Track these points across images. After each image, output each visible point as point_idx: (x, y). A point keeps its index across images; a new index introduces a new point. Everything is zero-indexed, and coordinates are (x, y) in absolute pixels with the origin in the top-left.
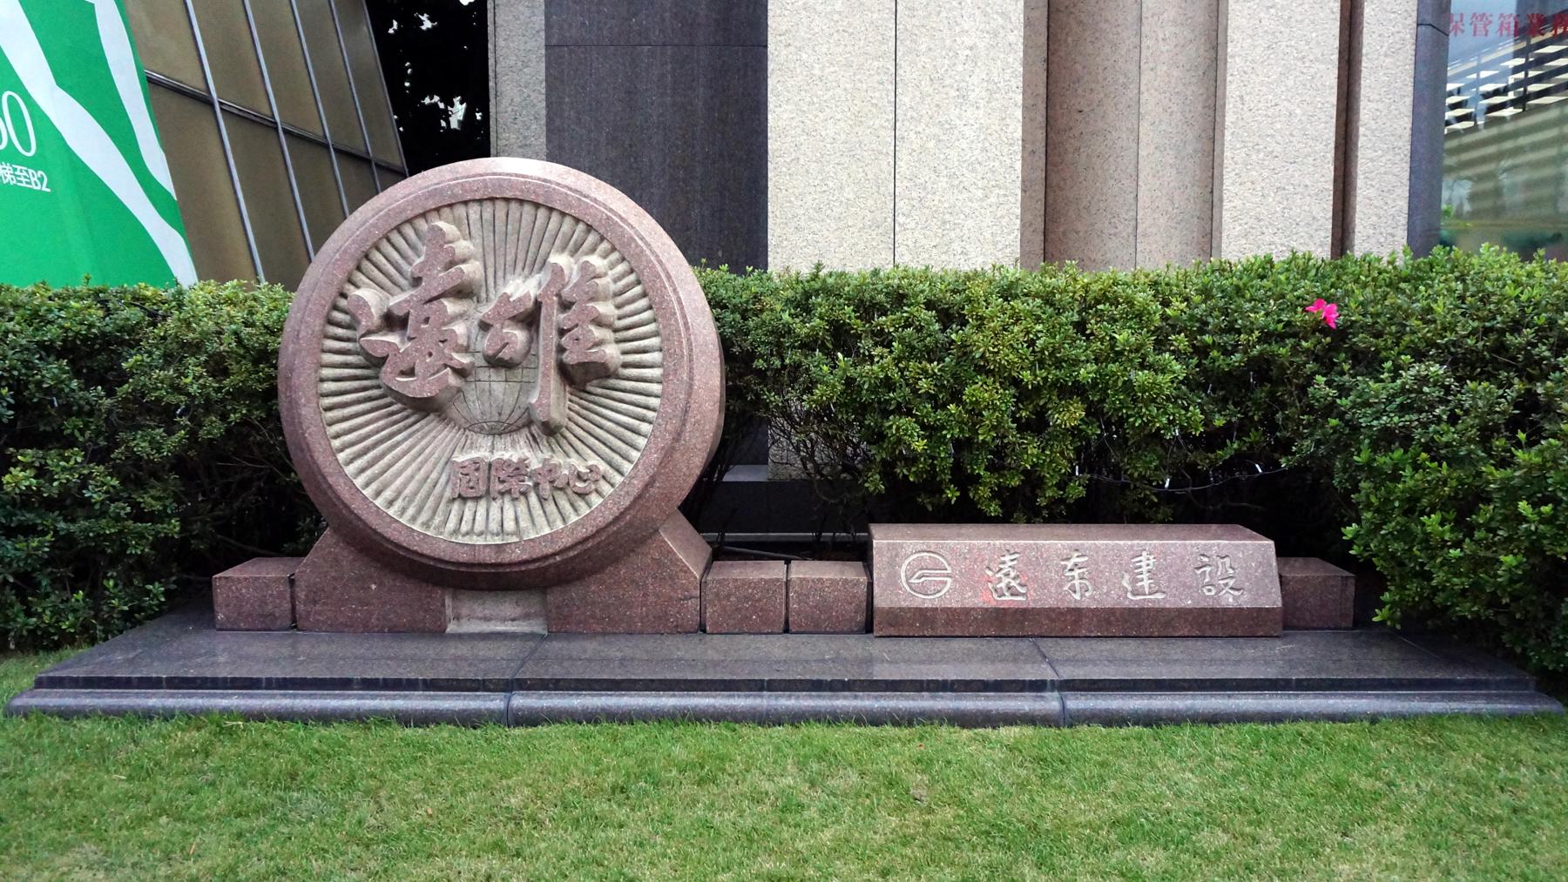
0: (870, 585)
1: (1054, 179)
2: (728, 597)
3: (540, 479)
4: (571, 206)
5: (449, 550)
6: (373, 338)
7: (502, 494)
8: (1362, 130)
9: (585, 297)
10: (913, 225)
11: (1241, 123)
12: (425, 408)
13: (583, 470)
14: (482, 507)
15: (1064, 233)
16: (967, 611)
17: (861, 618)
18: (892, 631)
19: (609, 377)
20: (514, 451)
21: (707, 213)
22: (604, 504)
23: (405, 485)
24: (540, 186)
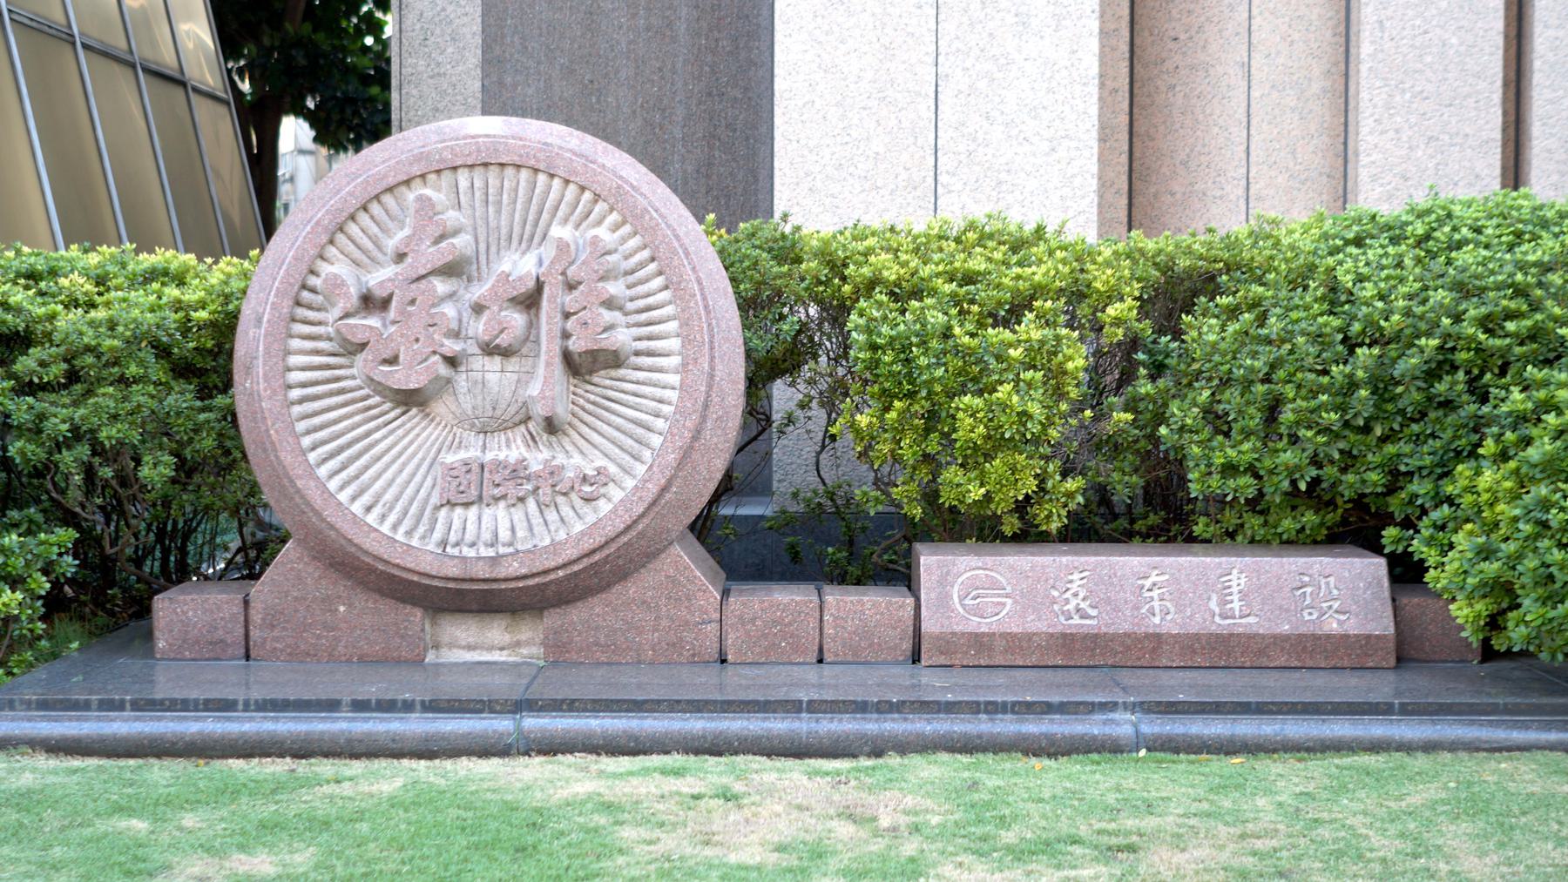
0: (918, 607)
1: (1140, 128)
2: (753, 621)
3: (541, 483)
4: (576, 174)
5: (436, 564)
6: (351, 321)
7: (497, 499)
8: (1537, 64)
9: (595, 277)
10: (959, 186)
11: (1380, 56)
12: (409, 399)
13: (591, 472)
14: (473, 512)
15: (1156, 196)
16: (1029, 637)
17: (907, 645)
18: (942, 660)
19: (618, 366)
20: (511, 449)
21: (690, 169)
22: (614, 511)
23: (385, 489)
24: (540, 150)
